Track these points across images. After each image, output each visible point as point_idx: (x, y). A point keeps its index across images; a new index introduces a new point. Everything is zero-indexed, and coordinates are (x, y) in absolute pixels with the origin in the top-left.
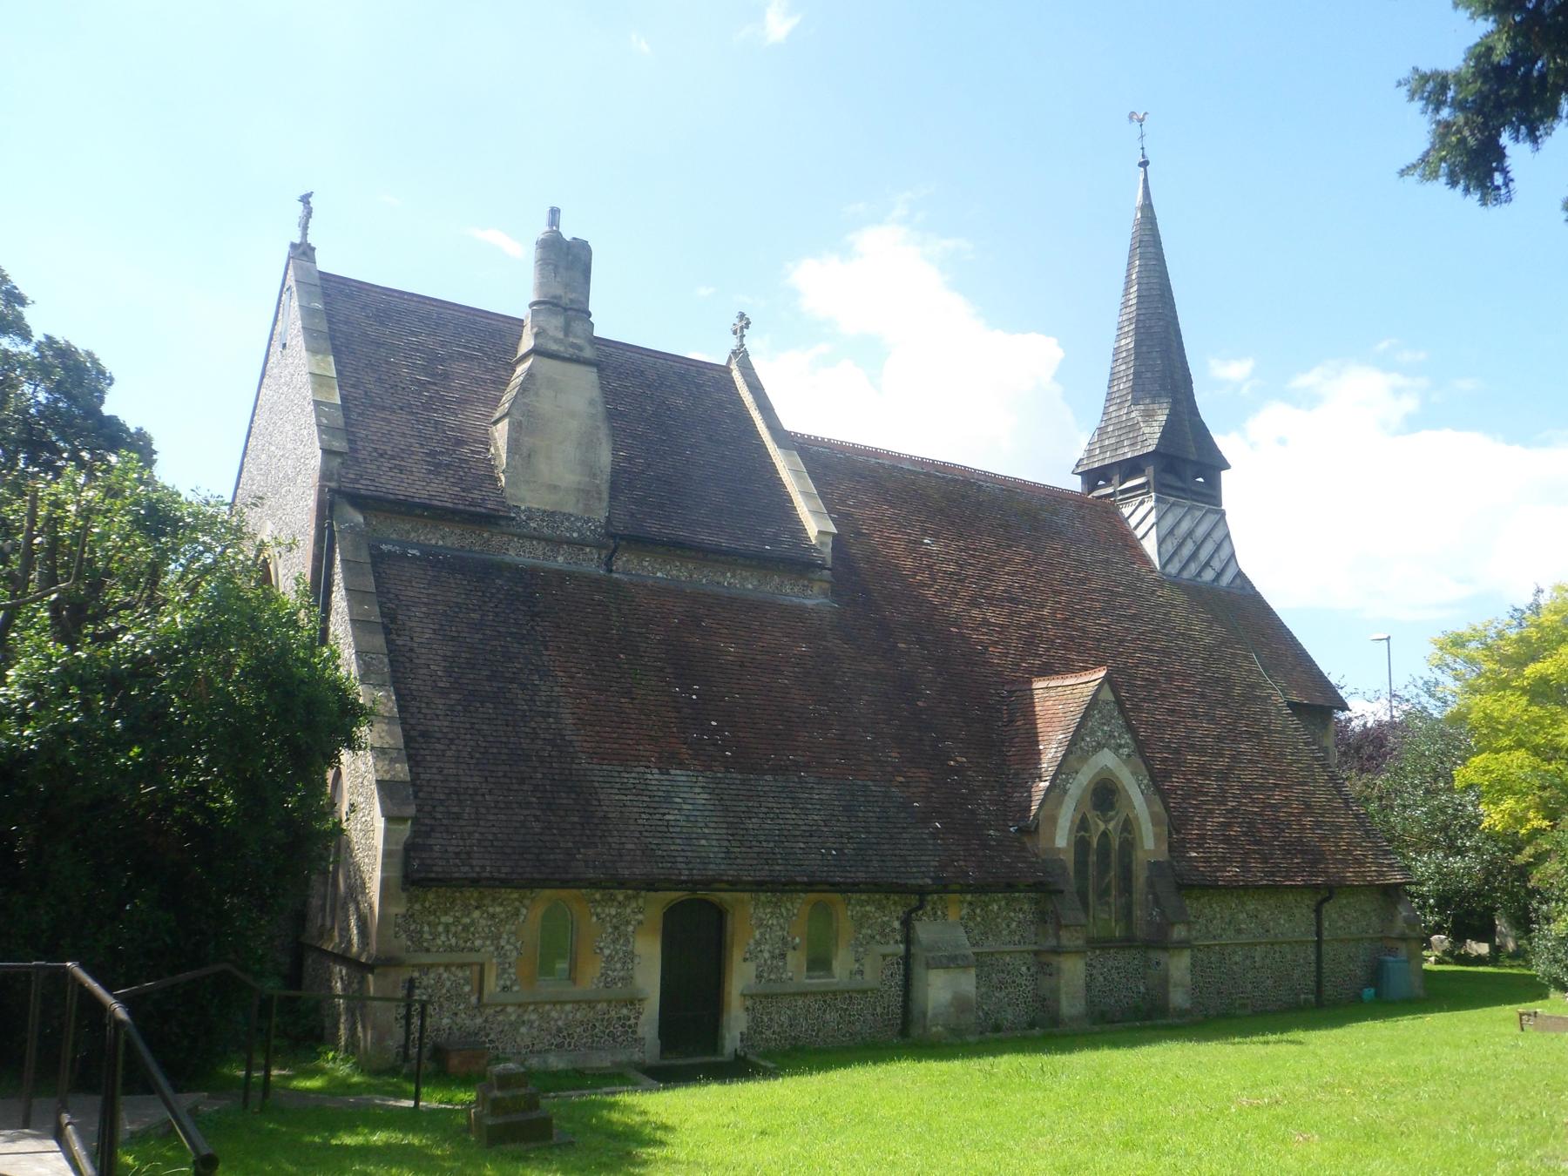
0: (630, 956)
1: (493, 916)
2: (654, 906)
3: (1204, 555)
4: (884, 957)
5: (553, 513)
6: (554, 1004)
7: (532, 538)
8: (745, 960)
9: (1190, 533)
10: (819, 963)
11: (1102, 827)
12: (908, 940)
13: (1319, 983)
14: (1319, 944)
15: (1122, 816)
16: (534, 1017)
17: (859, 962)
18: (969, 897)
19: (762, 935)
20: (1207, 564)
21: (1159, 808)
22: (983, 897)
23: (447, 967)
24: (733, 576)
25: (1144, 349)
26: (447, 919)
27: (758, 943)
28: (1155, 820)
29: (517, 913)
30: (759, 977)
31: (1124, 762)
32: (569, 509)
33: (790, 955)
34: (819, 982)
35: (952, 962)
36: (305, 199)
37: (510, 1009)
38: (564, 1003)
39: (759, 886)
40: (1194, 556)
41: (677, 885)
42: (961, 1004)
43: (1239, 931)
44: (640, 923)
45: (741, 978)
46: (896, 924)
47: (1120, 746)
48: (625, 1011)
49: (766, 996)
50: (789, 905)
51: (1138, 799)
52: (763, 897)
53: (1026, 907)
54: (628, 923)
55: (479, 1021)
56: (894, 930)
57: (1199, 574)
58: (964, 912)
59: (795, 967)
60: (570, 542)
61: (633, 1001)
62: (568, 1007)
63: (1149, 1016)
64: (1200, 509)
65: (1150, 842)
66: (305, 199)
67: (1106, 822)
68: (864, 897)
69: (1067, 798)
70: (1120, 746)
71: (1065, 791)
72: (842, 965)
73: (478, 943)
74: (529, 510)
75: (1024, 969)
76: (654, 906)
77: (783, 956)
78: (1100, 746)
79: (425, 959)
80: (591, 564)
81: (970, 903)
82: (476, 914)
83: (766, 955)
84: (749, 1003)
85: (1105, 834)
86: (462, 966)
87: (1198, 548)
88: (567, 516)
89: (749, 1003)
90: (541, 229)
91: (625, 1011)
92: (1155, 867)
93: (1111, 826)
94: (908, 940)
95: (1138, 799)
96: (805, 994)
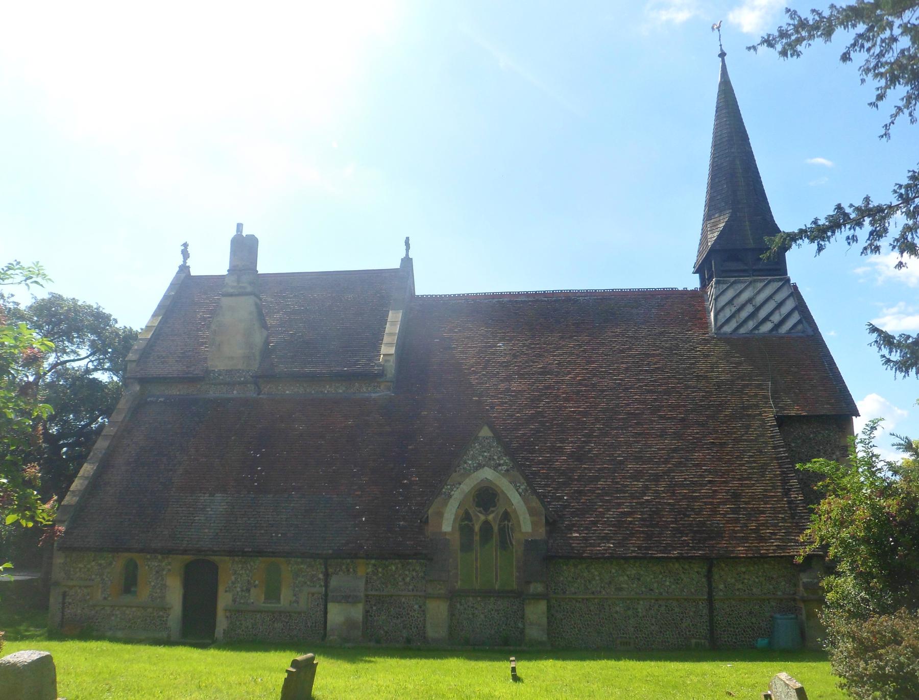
0: (164, 587)
1: (100, 565)
2: (177, 563)
3: (762, 314)
4: (313, 594)
5: (231, 371)
6: (127, 607)
7: (221, 384)
8: (226, 591)
9: (750, 301)
10: (273, 594)
11: (482, 518)
12: (326, 586)
13: (712, 631)
14: (710, 600)
15: (502, 511)
16: (118, 612)
17: (295, 594)
18: (373, 561)
19: (236, 579)
20: (766, 319)
21: (535, 503)
22: (384, 562)
23: (80, 587)
24: (330, 387)
25: (717, 180)
26: (81, 565)
27: (233, 583)
28: (532, 512)
29: (111, 564)
30: (234, 601)
31: (503, 475)
32: (240, 367)
33: (253, 590)
34: (271, 606)
35: (348, 599)
36: (886, 135)
37: (107, 608)
38: (131, 607)
39: (231, 553)
40: (752, 316)
41: (185, 552)
42: (350, 624)
43: (620, 589)
44: (169, 570)
45: (224, 600)
46: (321, 576)
47: (500, 465)
48: (161, 613)
49: (238, 611)
50: (252, 563)
51: (515, 499)
52: (236, 559)
53: (418, 568)
54: (163, 570)
55: (93, 612)
56: (319, 579)
57: (756, 328)
58: (370, 570)
59: (257, 597)
60: (240, 383)
61: (165, 609)
62: (134, 609)
63: (506, 642)
64: (761, 281)
65: (526, 525)
66: (886, 135)
67: (487, 514)
68: (299, 560)
69: (451, 501)
70: (500, 465)
71: (450, 496)
72: (286, 596)
73: (93, 577)
74: (219, 370)
75: (416, 607)
76: (177, 563)
77: (248, 590)
78: (480, 466)
79: (71, 583)
80: (251, 392)
81: (374, 565)
82: (93, 563)
83: (239, 589)
84: (228, 614)
85: (486, 522)
86: (86, 587)
87: (758, 309)
88: (238, 371)
89: (228, 614)
90: (233, 232)
91: (161, 613)
92: (530, 545)
93: (491, 517)
94: (326, 586)
95: (515, 499)
96: (261, 612)
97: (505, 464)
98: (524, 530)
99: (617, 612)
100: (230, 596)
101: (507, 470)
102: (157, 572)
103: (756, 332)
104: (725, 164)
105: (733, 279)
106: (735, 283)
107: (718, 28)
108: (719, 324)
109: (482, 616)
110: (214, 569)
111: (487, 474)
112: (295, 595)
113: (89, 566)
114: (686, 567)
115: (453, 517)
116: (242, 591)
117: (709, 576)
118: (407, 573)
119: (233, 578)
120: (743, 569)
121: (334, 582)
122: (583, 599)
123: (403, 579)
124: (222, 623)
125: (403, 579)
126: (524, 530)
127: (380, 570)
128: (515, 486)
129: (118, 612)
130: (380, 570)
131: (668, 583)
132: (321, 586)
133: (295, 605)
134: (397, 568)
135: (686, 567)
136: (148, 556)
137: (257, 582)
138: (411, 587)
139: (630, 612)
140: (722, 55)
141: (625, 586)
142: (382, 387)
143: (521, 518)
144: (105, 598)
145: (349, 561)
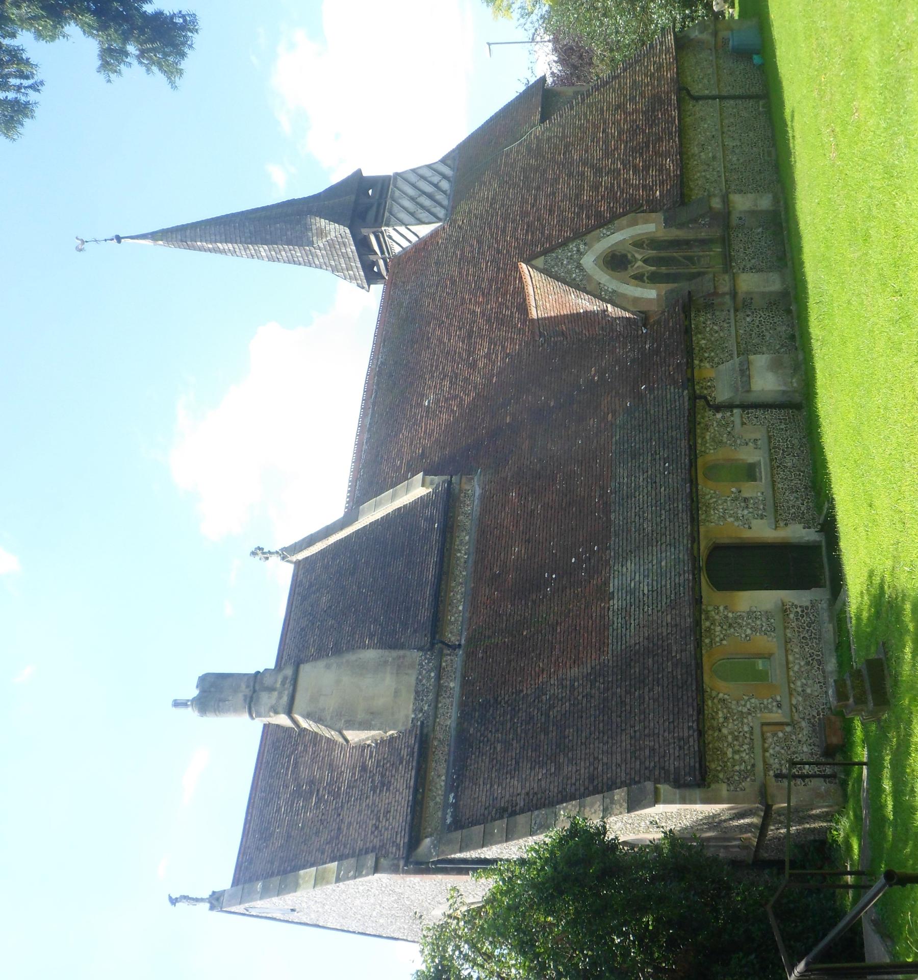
0: (750, 614)
2: (711, 596)
4: (743, 424)
5: (417, 692)
7: (436, 707)
9: (412, 199)
10: (750, 473)
11: (640, 263)
12: (730, 406)
13: (750, 97)
16: (799, 683)
17: (746, 443)
18: (696, 362)
21: (624, 221)
22: (696, 351)
23: (765, 750)
24: (459, 551)
27: (737, 519)
28: (634, 223)
30: (762, 517)
32: (413, 680)
33: (745, 494)
34: (764, 472)
37: (794, 702)
39: (695, 520)
40: (430, 196)
41: (696, 581)
42: (776, 366)
43: (714, 158)
44: (726, 608)
45: (763, 531)
46: (719, 416)
47: (578, 251)
49: (776, 511)
51: (617, 237)
54: (726, 617)
55: (803, 724)
56: (723, 418)
57: (444, 192)
58: (707, 365)
60: (439, 677)
61: (784, 610)
62: (791, 658)
64: (393, 192)
65: (650, 227)
67: (636, 260)
68: (699, 441)
70: (578, 251)
71: (614, 292)
73: (746, 729)
74: (414, 711)
76: (711, 596)
77: (746, 500)
78: (579, 266)
79: (760, 766)
80: (455, 661)
81: (701, 361)
83: (746, 512)
84: (782, 524)
85: (645, 261)
86: (764, 740)
88: (419, 681)
91: (792, 616)
92: (668, 223)
93: (639, 257)
95: (617, 237)
96: (774, 482)
97: (577, 246)
98: (654, 230)
99: (738, 160)
100: (756, 523)
101: (585, 244)
102: (730, 626)
103: (448, 192)
104: (252, 228)
105: (387, 214)
106: (391, 213)
107: (83, 242)
108: (435, 219)
109: (753, 261)
110: (717, 549)
111: (588, 261)
112: (747, 444)
113: (730, 738)
114: (689, 113)
115: (639, 289)
116: (747, 507)
117: (697, 99)
118: (708, 329)
119: (730, 520)
120: (689, 78)
121: (722, 394)
122: (726, 184)
123: (717, 332)
124: (797, 533)
125: (717, 332)
126: (654, 230)
127: (706, 355)
128: (603, 237)
129: (799, 683)
130: (706, 355)
131: (706, 126)
132: (732, 415)
133: (759, 442)
134: (704, 339)
135: (689, 113)
136: (707, 641)
137: (733, 490)
138: (726, 325)
139: (737, 151)
140: (119, 239)
141: (710, 155)
142: (467, 487)
143: (640, 232)
144: (779, 706)
145: (697, 387)
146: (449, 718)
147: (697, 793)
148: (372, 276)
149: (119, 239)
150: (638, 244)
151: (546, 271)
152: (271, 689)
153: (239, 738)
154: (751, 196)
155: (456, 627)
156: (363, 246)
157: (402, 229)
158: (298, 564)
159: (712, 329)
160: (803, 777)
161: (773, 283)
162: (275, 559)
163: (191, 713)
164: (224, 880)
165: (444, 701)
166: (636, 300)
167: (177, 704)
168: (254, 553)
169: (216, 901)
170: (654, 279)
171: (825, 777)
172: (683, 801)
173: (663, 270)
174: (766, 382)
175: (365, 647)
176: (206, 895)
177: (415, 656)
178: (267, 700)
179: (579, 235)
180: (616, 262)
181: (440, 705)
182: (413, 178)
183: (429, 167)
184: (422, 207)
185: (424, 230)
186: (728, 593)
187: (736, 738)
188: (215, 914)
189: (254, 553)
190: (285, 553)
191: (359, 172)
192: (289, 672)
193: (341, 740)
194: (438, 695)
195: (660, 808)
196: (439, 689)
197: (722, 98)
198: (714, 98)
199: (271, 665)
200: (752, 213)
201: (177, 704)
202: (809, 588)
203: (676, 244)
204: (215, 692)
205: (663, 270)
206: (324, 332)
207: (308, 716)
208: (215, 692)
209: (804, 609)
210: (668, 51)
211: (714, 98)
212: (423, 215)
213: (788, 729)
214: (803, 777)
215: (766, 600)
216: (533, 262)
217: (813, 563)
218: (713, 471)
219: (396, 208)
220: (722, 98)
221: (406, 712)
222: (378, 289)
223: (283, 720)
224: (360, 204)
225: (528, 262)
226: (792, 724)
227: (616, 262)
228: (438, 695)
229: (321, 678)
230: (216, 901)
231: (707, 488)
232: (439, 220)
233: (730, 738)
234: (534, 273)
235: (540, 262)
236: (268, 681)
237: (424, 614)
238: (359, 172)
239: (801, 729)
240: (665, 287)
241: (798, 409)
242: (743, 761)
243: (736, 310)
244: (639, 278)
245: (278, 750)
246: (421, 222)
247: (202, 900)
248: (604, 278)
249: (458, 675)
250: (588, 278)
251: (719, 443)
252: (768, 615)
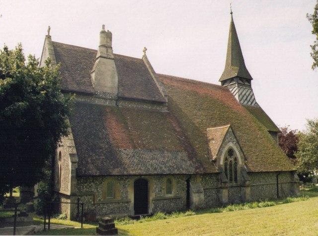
2: (131, 182)
9: (245, 94)
33: (162, 191)
43: (260, 182)
45: (152, 196)
61: (128, 202)
71: (222, 152)
77: (161, 191)
88: (109, 93)
102: (123, 185)
111: (231, 145)
113: (90, 185)
117: (277, 177)
140: (231, 13)
146: (97, 102)
147: (74, 175)
148: (224, 82)
149: (231, 13)
150: (236, 159)
151: (227, 132)
152: (107, 51)
153: (93, 42)
154: (250, 193)
155: (121, 104)
156: (232, 80)
157: (237, 91)
158: (142, 60)
159: (212, 183)
160: (78, 207)
161: (225, 199)
162: (143, 54)
163: (101, 29)
164: (53, 39)
165: (103, 100)
166: (220, 159)
167: (104, 26)
168: (145, 48)
169: (49, 37)
170: (226, 164)
171: (78, 213)
172: (72, 170)
173: (228, 167)
174: (196, 198)
175: (118, 78)
176: (50, 34)
177: (115, 92)
178: (104, 49)
179: (238, 142)
180: (231, 152)
181: (125, 173)
182: (251, 94)
183: (254, 99)
184: (243, 97)
185: (237, 97)
186: (133, 185)
187: (90, 187)
188: (44, 37)
189: (145, 48)
190: (145, 56)
191: (252, 79)
192: (113, 57)
193: (97, 57)
194: (104, 99)
195: (70, 164)
196: (106, 99)
197: (277, 184)
198: (277, 182)
199: (114, 52)
200: (245, 193)
201: (104, 26)
202: (134, 209)
203: (236, 172)
204: (107, 36)
205: (228, 167)
206: (210, 69)
207: (99, 62)
208: (107, 36)
209: (128, 208)
210: (290, 168)
211: (277, 182)
212: (241, 97)
213: (93, 202)
214: (78, 207)
215: (131, 197)
216: (230, 129)
217: (141, 210)
218: (170, 182)
219: (247, 90)
220: (277, 184)
221: (99, 90)
222: (220, 84)
223: (99, 55)
224: (244, 79)
225: (230, 127)
226: (94, 204)
227: (231, 152)
228: (104, 99)
229: (111, 65)
230: (49, 37)
231: (165, 180)
232: (240, 101)
233: (90, 185)
234: (227, 129)
235: (230, 130)
236: (109, 50)
237: (127, 95)
238: (252, 79)
239: (92, 207)
240: (223, 167)
241: (186, 206)
242: (83, 188)
243: (217, 188)
244: (226, 159)
245: (89, 55)
246: (239, 96)
247: (49, 33)
248: (226, 149)
249: (110, 105)
250: (226, 144)
251: (178, 183)
252: (127, 197)
